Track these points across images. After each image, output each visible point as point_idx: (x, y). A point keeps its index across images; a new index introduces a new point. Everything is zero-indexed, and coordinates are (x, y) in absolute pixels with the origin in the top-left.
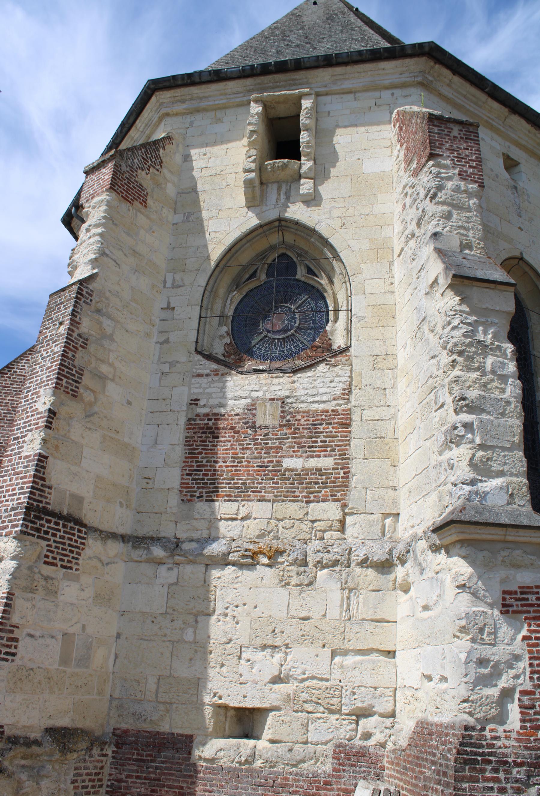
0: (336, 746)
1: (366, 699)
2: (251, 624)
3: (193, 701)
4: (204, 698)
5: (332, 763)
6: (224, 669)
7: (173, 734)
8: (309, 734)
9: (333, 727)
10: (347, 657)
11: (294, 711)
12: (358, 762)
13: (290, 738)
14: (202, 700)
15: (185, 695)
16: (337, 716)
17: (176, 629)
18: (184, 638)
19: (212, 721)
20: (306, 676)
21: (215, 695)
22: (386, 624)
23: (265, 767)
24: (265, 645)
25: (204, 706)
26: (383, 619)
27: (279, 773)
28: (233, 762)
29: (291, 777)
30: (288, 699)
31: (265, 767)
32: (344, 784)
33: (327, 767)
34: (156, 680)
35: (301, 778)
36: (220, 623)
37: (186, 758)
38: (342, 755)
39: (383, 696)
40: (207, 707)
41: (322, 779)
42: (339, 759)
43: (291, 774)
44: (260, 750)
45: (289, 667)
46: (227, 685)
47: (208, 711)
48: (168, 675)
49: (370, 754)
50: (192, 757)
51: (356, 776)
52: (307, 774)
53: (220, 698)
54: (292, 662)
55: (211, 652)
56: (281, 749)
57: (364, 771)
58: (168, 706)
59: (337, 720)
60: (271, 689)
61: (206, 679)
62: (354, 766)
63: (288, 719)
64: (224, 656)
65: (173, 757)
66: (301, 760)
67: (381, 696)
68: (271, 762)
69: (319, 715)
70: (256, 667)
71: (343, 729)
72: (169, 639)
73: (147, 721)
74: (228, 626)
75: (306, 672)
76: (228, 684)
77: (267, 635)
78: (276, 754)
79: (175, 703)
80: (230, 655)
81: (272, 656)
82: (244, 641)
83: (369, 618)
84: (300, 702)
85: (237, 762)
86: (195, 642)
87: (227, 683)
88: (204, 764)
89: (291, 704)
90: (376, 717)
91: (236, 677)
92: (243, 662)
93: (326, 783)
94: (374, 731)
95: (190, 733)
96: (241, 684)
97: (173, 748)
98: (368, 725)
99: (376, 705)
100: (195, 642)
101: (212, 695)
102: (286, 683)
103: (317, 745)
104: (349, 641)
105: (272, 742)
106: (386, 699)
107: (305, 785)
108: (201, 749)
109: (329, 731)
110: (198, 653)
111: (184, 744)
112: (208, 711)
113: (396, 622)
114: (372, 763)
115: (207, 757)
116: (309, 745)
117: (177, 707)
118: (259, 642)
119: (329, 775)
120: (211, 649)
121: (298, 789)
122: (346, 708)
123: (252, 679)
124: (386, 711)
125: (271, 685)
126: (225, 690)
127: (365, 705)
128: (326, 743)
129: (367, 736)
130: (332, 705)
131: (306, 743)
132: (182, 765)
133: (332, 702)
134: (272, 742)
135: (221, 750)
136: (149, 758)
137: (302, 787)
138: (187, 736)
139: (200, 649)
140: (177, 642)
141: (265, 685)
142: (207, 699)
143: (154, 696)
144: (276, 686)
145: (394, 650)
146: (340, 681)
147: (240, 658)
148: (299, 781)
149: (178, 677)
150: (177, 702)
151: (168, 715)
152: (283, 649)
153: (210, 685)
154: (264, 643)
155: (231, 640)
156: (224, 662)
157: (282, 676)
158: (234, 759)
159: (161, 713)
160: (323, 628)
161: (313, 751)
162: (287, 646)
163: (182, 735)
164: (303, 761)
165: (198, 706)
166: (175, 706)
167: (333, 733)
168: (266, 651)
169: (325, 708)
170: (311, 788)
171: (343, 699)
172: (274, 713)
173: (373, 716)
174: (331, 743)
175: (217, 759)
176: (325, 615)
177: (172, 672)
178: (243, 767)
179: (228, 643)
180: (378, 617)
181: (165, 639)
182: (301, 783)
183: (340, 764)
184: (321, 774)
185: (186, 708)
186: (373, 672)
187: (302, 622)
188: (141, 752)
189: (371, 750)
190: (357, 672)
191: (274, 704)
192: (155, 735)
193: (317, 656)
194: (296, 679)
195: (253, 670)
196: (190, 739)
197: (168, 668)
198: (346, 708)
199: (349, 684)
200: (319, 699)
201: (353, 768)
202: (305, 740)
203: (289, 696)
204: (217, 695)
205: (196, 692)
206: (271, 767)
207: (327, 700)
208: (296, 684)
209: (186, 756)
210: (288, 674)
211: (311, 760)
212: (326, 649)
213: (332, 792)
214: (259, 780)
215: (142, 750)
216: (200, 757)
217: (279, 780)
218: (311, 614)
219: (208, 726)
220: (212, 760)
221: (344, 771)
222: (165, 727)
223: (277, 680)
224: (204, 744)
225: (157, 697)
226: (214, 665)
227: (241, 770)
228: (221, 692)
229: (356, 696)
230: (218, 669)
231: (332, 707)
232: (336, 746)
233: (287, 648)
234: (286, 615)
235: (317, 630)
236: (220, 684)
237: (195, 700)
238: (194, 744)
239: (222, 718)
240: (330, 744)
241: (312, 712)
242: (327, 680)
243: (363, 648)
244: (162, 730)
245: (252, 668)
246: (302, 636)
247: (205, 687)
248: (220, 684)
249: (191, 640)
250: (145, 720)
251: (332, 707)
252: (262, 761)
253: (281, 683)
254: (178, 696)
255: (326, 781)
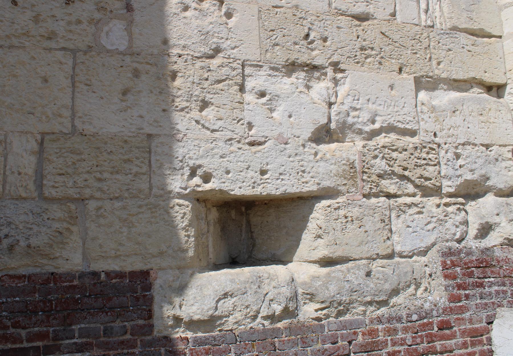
0: (445, 254)
1: (477, 165)
2: (259, 18)
3: (140, 191)
4: (169, 181)
5: (446, 287)
6: (209, 113)
7: (95, 274)
8: (395, 237)
9: (434, 220)
10: (437, 93)
11: (364, 196)
12: (485, 277)
13: (366, 250)
14: (163, 187)
15: (118, 177)
16: (435, 200)
17: (79, 22)
18: (104, 41)
19: (192, 232)
20: (377, 126)
21: (193, 174)
22: (486, 40)
23: (327, 316)
24: (293, 64)
25: (169, 199)
26: (482, 30)
27: (360, 324)
28: (255, 317)
29: (380, 327)
30: (352, 172)
31: (327, 316)
32: (471, 321)
33: (435, 295)
34: (34, 145)
35: (399, 326)
36: (188, 14)
37: (142, 327)
38: (458, 269)
39: (500, 159)
40: (177, 201)
41: (436, 320)
42: (455, 278)
43: (379, 320)
44: (304, 283)
45: (345, 107)
46: (222, 147)
47: (182, 212)
48: (67, 128)
49: (499, 262)
50: (156, 322)
51: (486, 304)
52: (409, 315)
53: (207, 178)
54: (350, 98)
55: (174, 76)
56: (350, 274)
57: (497, 292)
58: (73, 207)
59: (438, 206)
60: (316, 154)
61: (173, 136)
62: (481, 285)
63: (355, 212)
64: (206, 84)
65: (108, 332)
66: (393, 290)
67: (497, 160)
68: (340, 304)
69: (408, 200)
70: (281, 108)
71: (450, 222)
72: (62, 45)
73: (17, 249)
74: (209, 19)
75: (377, 118)
76: (217, 149)
77: (296, 44)
78: (347, 286)
79: (92, 197)
80: (219, 82)
81: (308, 87)
82: (250, 52)
83: (463, 26)
84: (374, 178)
85: (265, 318)
86: (131, 52)
87: (221, 144)
88: (189, 335)
89: (359, 180)
90: (490, 199)
91: (240, 129)
92: (249, 97)
93: (444, 326)
94: (497, 219)
95: (138, 266)
96: (252, 144)
97: (101, 309)
98: (484, 212)
99: (493, 175)
100: (131, 52)
101: (187, 172)
102: (338, 141)
103: (411, 257)
104: (439, 64)
105: (327, 262)
106: (504, 164)
107: (409, 337)
108: (177, 300)
109: (421, 229)
110: (143, 77)
111: (133, 295)
112: (182, 212)
113: (500, 37)
114: (505, 277)
115: (196, 317)
116: (397, 259)
117: (99, 208)
118: (280, 56)
119: (445, 310)
120: (175, 67)
121: (397, 348)
122: (449, 183)
123: (276, 133)
124: (507, 186)
125: (314, 145)
126: (217, 160)
127: (475, 177)
128: (424, 253)
129: (485, 230)
130: (427, 179)
131: (390, 256)
132: (134, 347)
133: (426, 174)
134: (327, 262)
135: (225, 295)
136: (40, 344)
137: (403, 342)
138: (133, 274)
139: (149, 69)
140: (85, 53)
141: (304, 146)
142: (176, 183)
143: (32, 187)
144: (323, 148)
145: (504, 82)
146: (435, 135)
147: (242, 89)
148: (395, 330)
149: (94, 135)
150: (98, 195)
151: (74, 229)
152: (330, 71)
153: (180, 150)
154: (293, 58)
155: (217, 51)
156: (208, 97)
157: (333, 126)
158: (258, 312)
159: (56, 225)
160: (396, 37)
161: (409, 269)
162: (336, 67)
163: (120, 275)
164: (395, 292)
165: (152, 200)
166: (92, 205)
167: (436, 231)
168: (295, 75)
169: (416, 186)
170: (418, 340)
171: (443, 167)
172: (325, 203)
173: (483, 196)
174: (436, 248)
175: (220, 317)
176: (393, 15)
177: (77, 123)
178: (280, 325)
179: (212, 57)
180: (475, 26)
181: (53, 44)
182: (400, 335)
183: (460, 287)
184: (432, 310)
185: (124, 208)
186: (481, 118)
187: (357, 23)
188: (12, 330)
189: (498, 253)
190: (457, 119)
191: (326, 183)
192: (47, 281)
193: (392, 87)
194: (360, 132)
195: (274, 115)
196: (143, 278)
197: (67, 113)
198: (449, 183)
199: (449, 140)
200: (405, 169)
201: (480, 290)
202: (389, 251)
203: (352, 166)
204: (199, 172)
205: (145, 169)
206: (340, 314)
207: (419, 171)
208: (360, 143)
209: (141, 322)
210: (344, 122)
211: (409, 286)
212: (404, 75)
213: (453, 341)
214: (319, 346)
215: (16, 325)
216: (178, 320)
217: (360, 338)
218: (371, 9)
219: (185, 246)
220: (210, 322)
221: (467, 297)
222: (72, 260)
223: (324, 134)
224: (181, 289)
225: (40, 186)
226: (185, 104)
227: (276, 332)
228: (209, 164)
229: (461, 162)
230: (195, 114)
231: (427, 183)
232: (445, 254)
233: (335, 71)
234: (326, 8)
235: (385, 39)
236: (205, 146)
237: (145, 186)
238: (156, 292)
239: (204, 226)
240: (433, 253)
241: (395, 196)
242: (413, 133)
243: (461, 76)
244: (63, 267)
245: (272, 110)
246: (362, 49)
247: (170, 156)
248: (205, 146)
249: (122, 48)
250: (11, 248)
251: (427, 183)
252: (318, 306)
253: (329, 142)
254: (100, 180)
255: (442, 322)
